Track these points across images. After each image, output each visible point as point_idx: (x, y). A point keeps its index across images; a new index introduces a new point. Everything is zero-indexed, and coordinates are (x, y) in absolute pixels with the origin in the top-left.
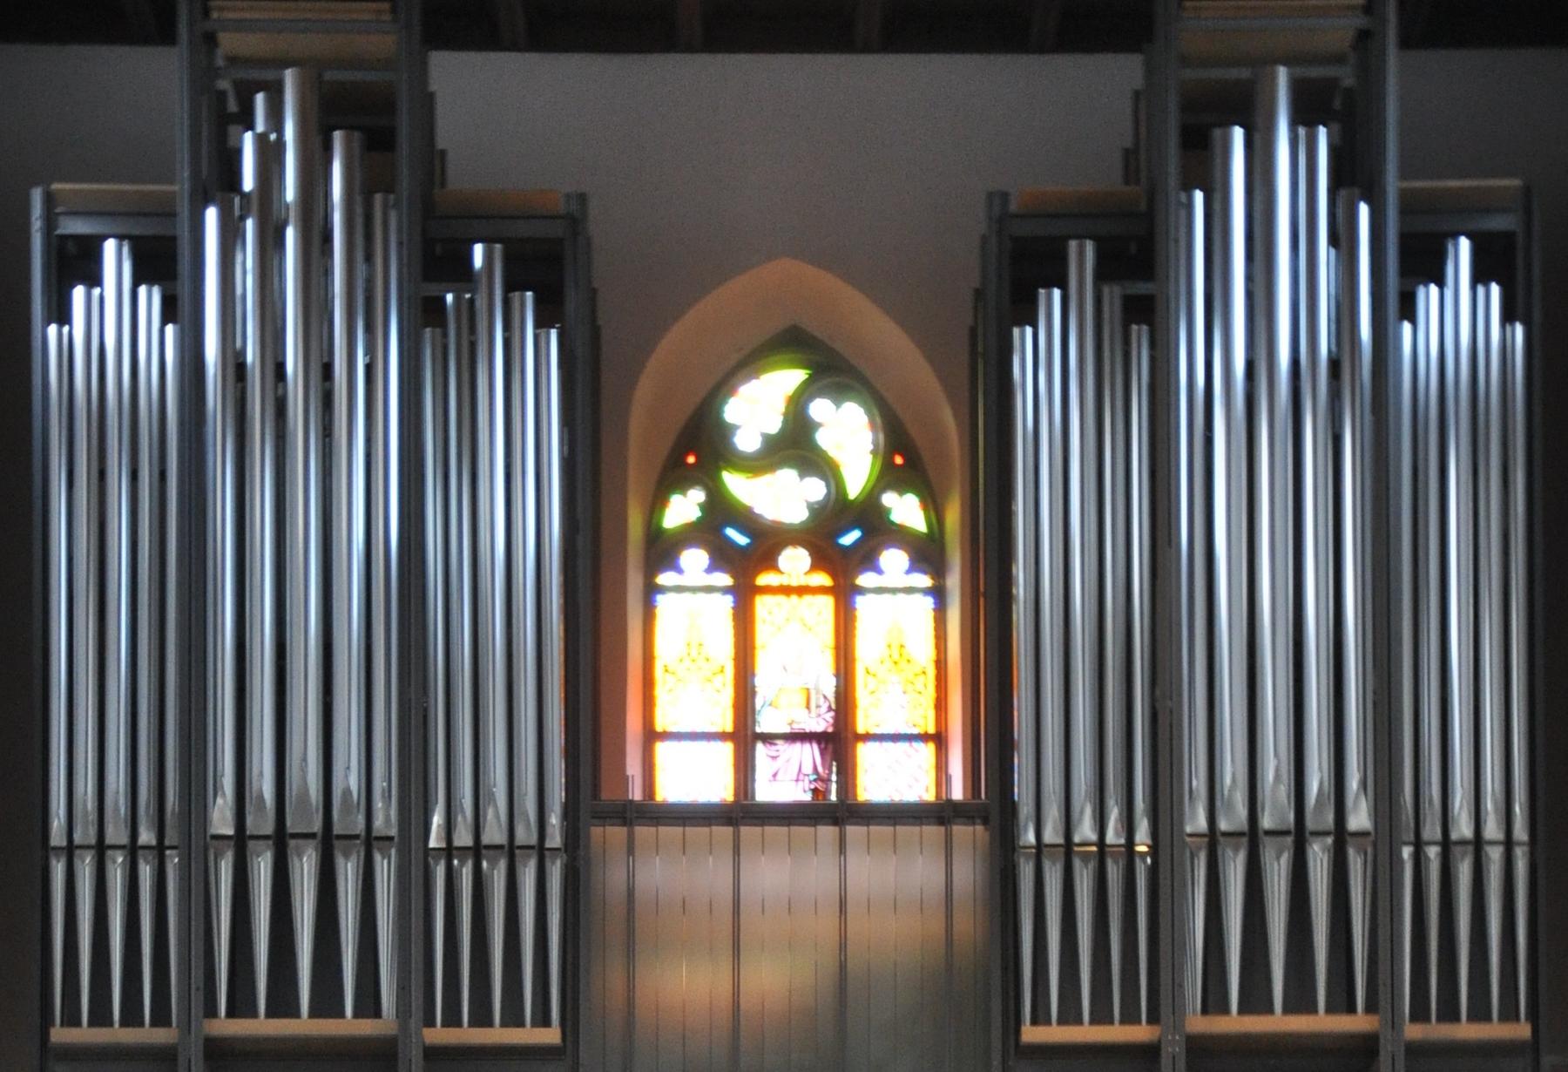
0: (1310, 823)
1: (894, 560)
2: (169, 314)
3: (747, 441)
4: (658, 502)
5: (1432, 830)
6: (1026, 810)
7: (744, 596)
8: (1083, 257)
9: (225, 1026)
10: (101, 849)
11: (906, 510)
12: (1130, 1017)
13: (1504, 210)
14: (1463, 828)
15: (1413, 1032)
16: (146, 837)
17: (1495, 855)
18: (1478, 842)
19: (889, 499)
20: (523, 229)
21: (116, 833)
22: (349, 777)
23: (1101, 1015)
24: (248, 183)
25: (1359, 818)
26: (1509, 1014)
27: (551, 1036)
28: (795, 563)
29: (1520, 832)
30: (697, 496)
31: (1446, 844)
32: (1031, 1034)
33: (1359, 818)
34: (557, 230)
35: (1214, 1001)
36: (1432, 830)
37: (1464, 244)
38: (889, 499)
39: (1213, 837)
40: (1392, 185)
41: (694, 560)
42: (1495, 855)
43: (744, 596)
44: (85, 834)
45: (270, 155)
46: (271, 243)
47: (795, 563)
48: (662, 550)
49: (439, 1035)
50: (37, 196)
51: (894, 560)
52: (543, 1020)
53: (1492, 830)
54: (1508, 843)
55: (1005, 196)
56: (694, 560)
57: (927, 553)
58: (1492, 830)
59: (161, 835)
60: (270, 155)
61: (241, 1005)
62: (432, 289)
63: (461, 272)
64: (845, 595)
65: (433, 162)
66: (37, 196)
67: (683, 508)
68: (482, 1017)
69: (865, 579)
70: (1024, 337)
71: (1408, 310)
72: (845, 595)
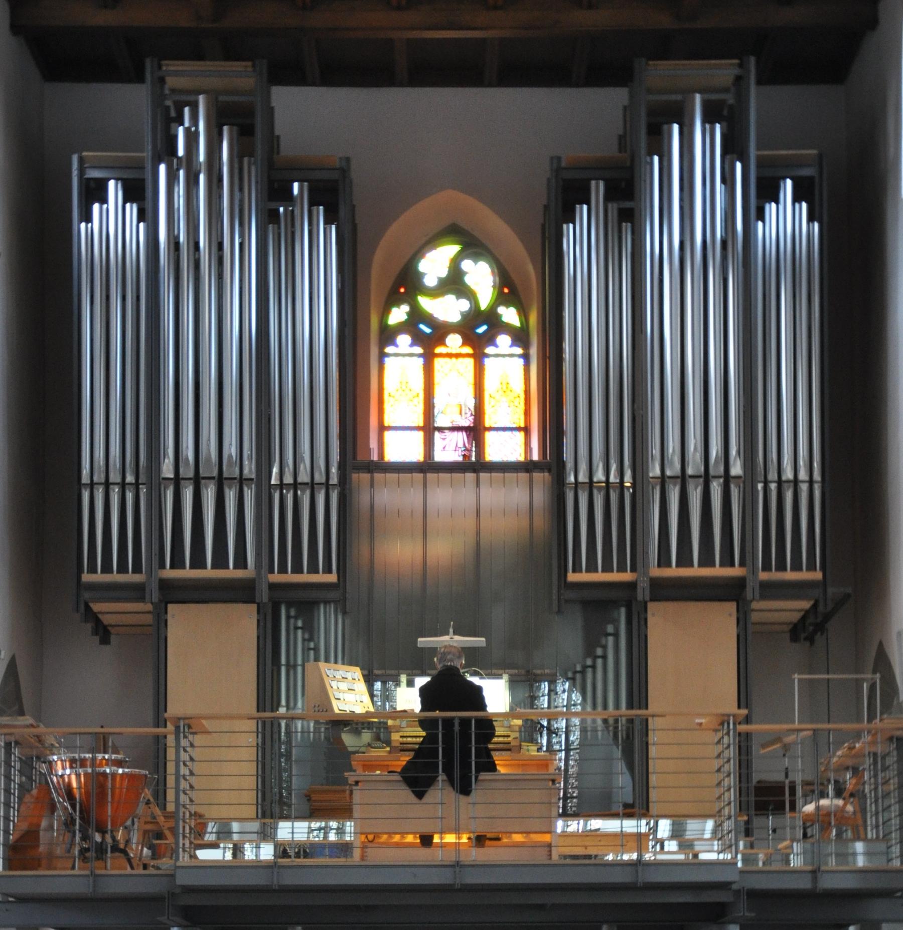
0: (712, 472)
1: (504, 341)
2: (141, 217)
3: (430, 281)
4: (385, 312)
5: (773, 475)
6: (570, 465)
7: (429, 358)
8: (598, 189)
9: (169, 573)
10: (107, 485)
11: (510, 315)
12: (622, 569)
13: (809, 166)
14: (788, 474)
15: (763, 576)
16: (130, 478)
17: (804, 487)
18: (796, 481)
19: (501, 310)
20: (318, 175)
21: (115, 477)
22: (231, 449)
23: (607, 568)
24: (181, 152)
25: (737, 469)
26: (811, 567)
27: (332, 578)
28: (454, 342)
29: (817, 476)
30: (405, 308)
31: (780, 482)
32: (572, 577)
33: (737, 469)
34: (335, 175)
35: (663, 561)
36: (773, 475)
37: (789, 182)
38: (501, 310)
39: (663, 479)
40: (753, 153)
41: (404, 340)
42: (804, 487)
43: (429, 358)
44: (99, 477)
45: (192, 138)
46: (191, 182)
47: (454, 342)
48: (388, 336)
49: (276, 577)
50: (75, 159)
51: (504, 341)
52: (328, 570)
53: (803, 475)
54: (811, 482)
55: (559, 159)
56: (404, 340)
57: (520, 337)
58: (803, 475)
59: (137, 478)
60: (192, 138)
61: (177, 563)
62: (272, 205)
63: (286, 196)
64: (479, 358)
65: (273, 141)
66: (75, 159)
67: (398, 315)
68: (298, 569)
69: (489, 350)
71: (761, 216)
72: (479, 358)
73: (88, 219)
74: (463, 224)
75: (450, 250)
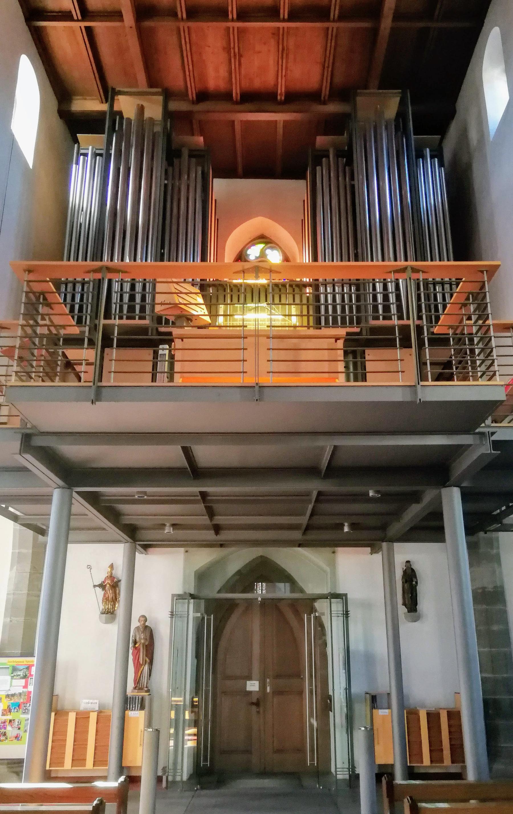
70: (318, 168)
73: (77, 163)
74: (267, 234)
75: (260, 246)
